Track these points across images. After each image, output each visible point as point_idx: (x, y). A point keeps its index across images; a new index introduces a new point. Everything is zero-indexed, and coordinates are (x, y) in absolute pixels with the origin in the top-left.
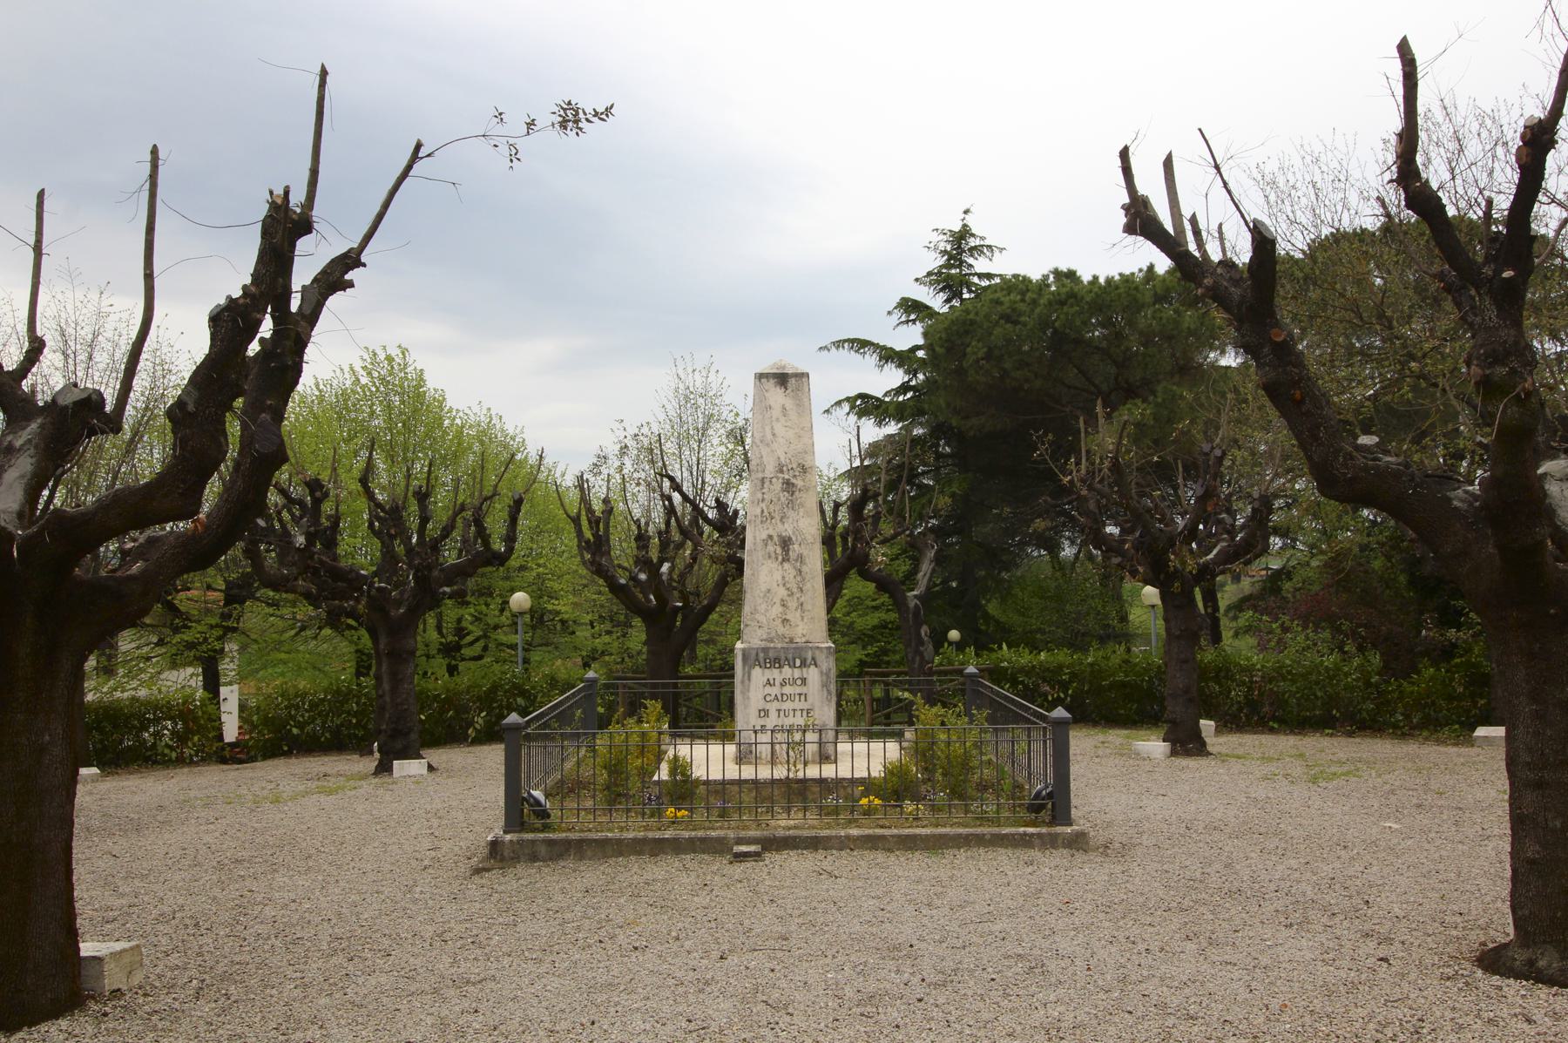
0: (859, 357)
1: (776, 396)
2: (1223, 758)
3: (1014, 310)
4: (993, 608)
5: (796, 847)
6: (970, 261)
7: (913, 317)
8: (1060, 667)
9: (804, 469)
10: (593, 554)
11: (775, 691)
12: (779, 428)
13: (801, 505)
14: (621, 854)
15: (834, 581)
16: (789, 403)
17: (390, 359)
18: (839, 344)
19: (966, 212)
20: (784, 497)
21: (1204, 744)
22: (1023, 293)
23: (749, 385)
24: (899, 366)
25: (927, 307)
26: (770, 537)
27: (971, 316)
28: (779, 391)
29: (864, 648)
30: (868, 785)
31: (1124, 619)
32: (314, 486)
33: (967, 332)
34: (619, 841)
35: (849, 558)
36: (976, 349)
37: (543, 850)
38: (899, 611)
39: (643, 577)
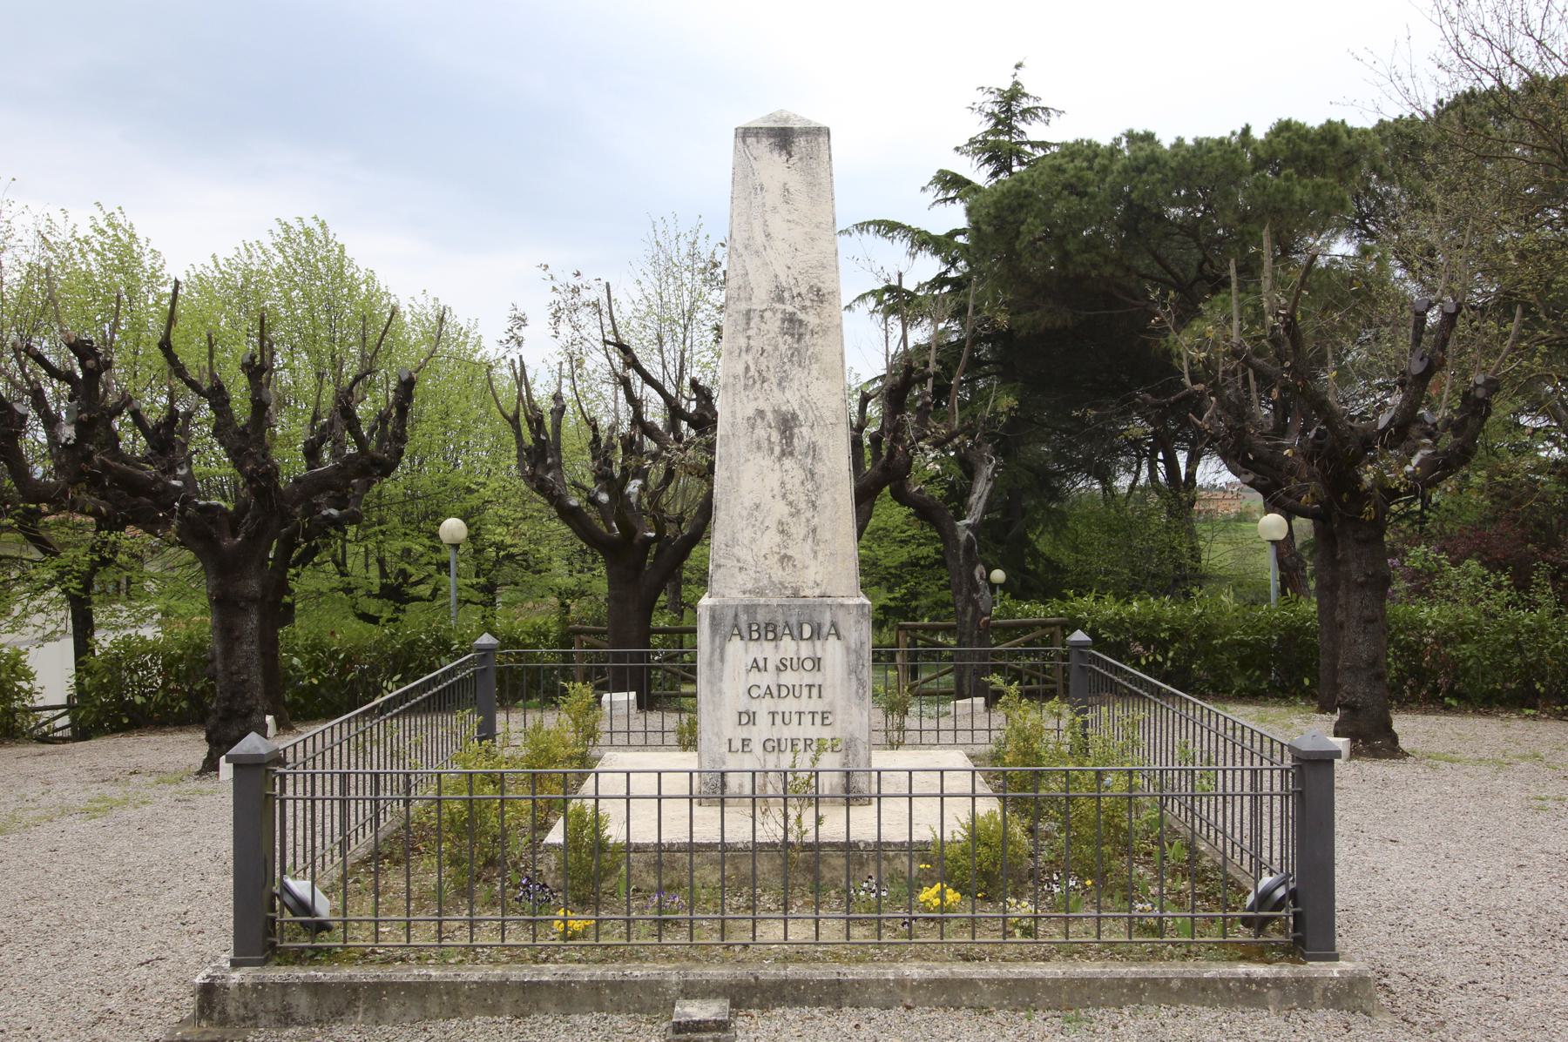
0: (886, 242)
1: (772, 166)
2: (1429, 759)
3: (1080, 179)
4: (1044, 544)
5: (797, 1001)
6: (1022, 126)
7: (952, 194)
8: (1157, 621)
9: (820, 296)
10: (534, 466)
11: (766, 679)
12: (777, 225)
13: (815, 358)
14: (456, 1012)
15: (865, 497)
16: (795, 181)
17: (308, 234)
18: (862, 227)
19: (1018, 66)
20: (785, 344)
21: (1394, 738)
22: (1090, 160)
23: (725, 148)
24: (936, 252)
25: (969, 182)
26: (761, 413)
27: (1027, 187)
28: (778, 159)
29: (890, 590)
30: (932, 860)
31: (1195, 553)
32: (82, 349)
33: (1021, 206)
34: (452, 988)
35: (885, 469)
36: (1032, 227)
37: (302, 1003)
38: (943, 540)
39: (604, 498)
